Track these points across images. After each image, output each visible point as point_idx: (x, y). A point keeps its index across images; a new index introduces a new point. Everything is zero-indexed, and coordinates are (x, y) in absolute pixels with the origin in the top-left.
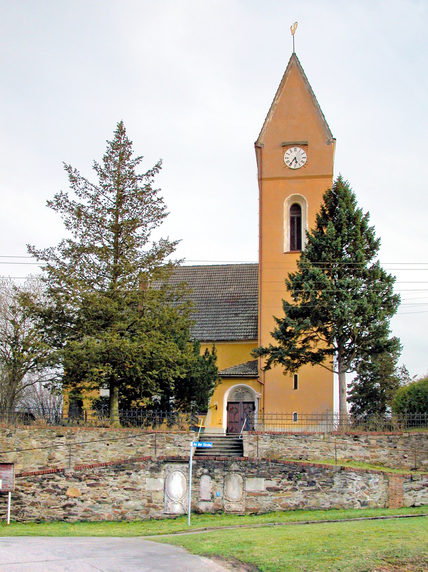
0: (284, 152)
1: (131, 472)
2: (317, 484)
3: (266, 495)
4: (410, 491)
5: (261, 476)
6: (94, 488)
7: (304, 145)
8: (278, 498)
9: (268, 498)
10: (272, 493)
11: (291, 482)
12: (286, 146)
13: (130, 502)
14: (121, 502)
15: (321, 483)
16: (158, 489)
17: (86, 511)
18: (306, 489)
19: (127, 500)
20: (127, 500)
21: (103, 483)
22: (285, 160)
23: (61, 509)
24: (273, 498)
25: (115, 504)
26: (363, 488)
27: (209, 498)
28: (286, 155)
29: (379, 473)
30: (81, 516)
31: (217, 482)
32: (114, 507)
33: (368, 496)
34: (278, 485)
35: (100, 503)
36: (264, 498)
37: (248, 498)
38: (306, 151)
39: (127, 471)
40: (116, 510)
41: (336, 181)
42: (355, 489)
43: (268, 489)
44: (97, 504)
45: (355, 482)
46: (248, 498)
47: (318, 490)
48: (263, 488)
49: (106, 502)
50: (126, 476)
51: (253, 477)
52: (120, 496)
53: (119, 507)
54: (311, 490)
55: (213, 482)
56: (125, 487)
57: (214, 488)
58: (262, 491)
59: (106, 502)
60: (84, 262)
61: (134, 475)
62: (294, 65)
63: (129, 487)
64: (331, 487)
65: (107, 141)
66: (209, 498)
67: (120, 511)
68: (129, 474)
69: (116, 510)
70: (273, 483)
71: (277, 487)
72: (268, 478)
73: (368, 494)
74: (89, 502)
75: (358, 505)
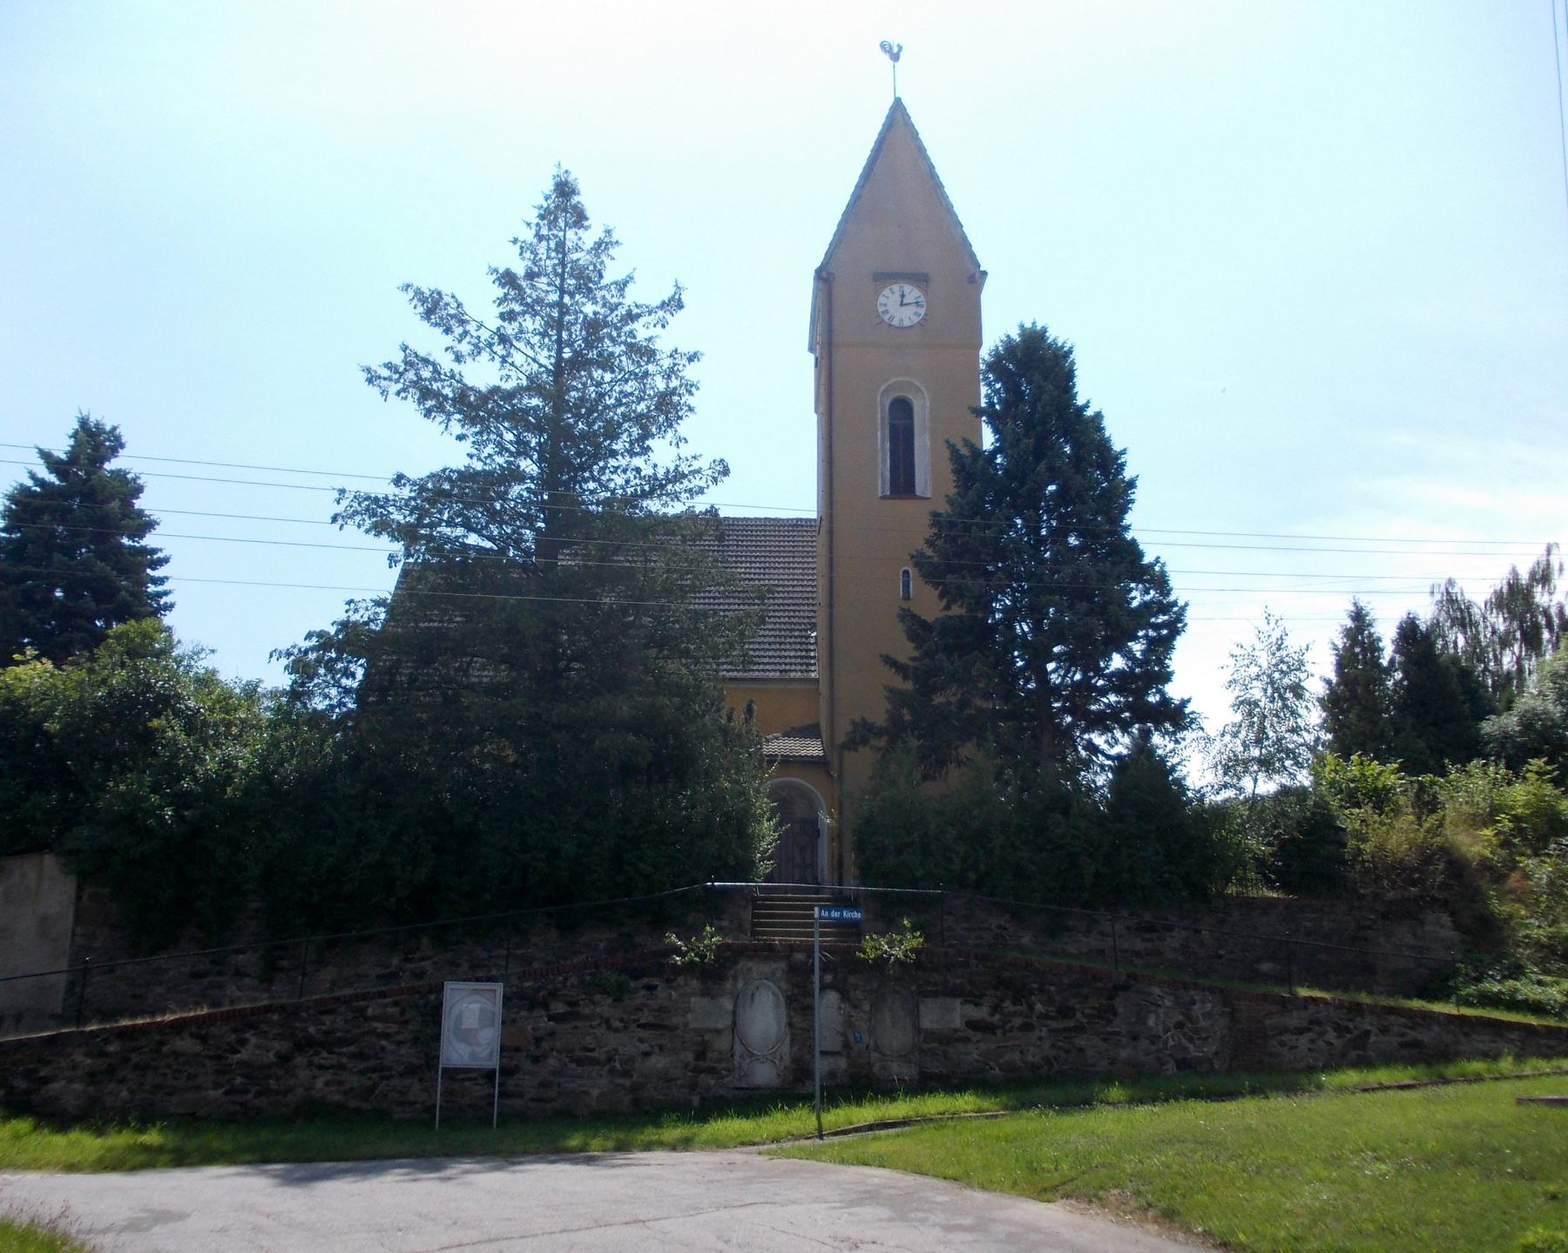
0: (877, 293)
1: (656, 981)
2: (1079, 1015)
3: (966, 1040)
4: (1281, 1034)
5: (952, 993)
6: (566, 1026)
7: (920, 279)
8: (993, 1046)
9: (971, 1047)
10: (979, 1036)
11: (1019, 1008)
12: (884, 278)
13: (653, 1060)
14: (631, 1059)
15: (1087, 1011)
16: (720, 1026)
17: (544, 1085)
18: (1054, 1024)
19: (646, 1054)
20: (646, 1054)
21: (587, 1011)
22: (881, 309)
23: (481, 1081)
24: (983, 1046)
25: (617, 1065)
26: (1180, 1025)
27: (838, 1048)
28: (881, 300)
29: (1211, 990)
30: (533, 1099)
31: (855, 1007)
32: (612, 1071)
33: (1191, 1047)
34: (992, 1015)
35: (579, 1062)
36: (960, 1047)
37: (926, 1046)
38: (925, 292)
39: (645, 981)
40: (620, 1081)
41: (987, 357)
42: (1161, 1028)
43: (972, 1025)
44: (574, 1066)
45: (1161, 1011)
46: (926, 1046)
47: (1080, 1029)
48: (958, 1022)
49: (594, 1062)
50: (643, 992)
51: (935, 995)
52: (626, 1044)
53: (626, 1074)
54: (1065, 1030)
55: (846, 1006)
56: (642, 1021)
57: (849, 1023)
58: (956, 1030)
59: (594, 1062)
60: (431, 621)
61: (662, 992)
62: (898, 109)
63: (651, 1019)
64: (1110, 1022)
65: (515, 241)
66: (838, 1048)
67: (627, 1083)
68: (651, 988)
69: (620, 1081)
70: (981, 1013)
71: (989, 1019)
72: (974, 998)
73: (1191, 1040)
74: (552, 1062)
75: (1171, 1067)
